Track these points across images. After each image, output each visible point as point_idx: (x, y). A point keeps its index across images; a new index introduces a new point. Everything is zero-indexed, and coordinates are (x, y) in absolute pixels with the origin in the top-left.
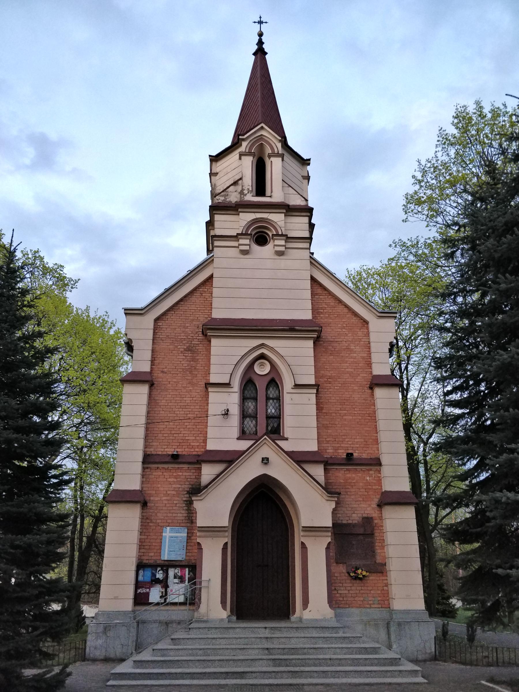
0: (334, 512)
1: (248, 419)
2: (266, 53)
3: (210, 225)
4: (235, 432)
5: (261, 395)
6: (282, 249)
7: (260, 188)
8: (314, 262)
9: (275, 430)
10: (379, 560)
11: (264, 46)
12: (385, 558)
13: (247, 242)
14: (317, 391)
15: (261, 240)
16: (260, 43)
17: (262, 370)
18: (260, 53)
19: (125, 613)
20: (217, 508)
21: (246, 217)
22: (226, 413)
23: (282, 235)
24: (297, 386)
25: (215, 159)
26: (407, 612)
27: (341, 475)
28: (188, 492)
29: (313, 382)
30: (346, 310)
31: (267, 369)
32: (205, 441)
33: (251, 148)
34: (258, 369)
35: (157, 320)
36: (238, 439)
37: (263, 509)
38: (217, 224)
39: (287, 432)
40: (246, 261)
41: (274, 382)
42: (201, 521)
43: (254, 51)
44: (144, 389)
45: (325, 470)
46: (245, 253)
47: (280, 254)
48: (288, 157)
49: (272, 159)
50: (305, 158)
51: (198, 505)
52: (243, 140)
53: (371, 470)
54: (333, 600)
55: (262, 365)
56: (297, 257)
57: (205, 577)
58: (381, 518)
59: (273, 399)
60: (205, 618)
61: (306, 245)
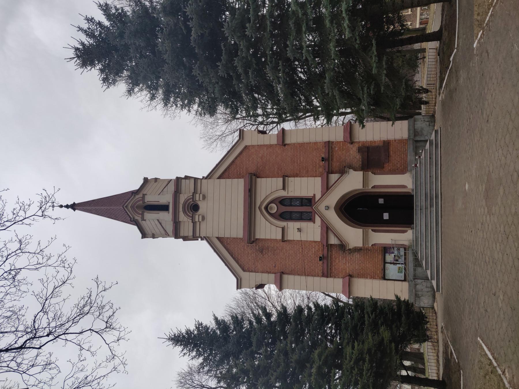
0: (355, 170)
1: (303, 217)
2: (74, 203)
3: (185, 239)
4: (310, 224)
5: (296, 209)
6: (201, 195)
7: (164, 208)
8: (209, 176)
9: (309, 201)
10: (381, 144)
11: (69, 204)
12: (380, 141)
13: (197, 217)
14: (286, 176)
15: (195, 208)
16: (67, 206)
17: (274, 208)
18: (74, 207)
19: (409, 286)
20: (353, 235)
21: (182, 217)
22: (299, 230)
23: (193, 195)
24: (284, 188)
25: (144, 235)
26: (409, 130)
27: (336, 165)
28: (344, 252)
29: (282, 179)
30: (239, 158)
31: (273, 205)
32: (315, 242)
33: (139, 214)
34: (274, 211)
35: (244, 270)
36: (314, 223)
37: (360, 209)
38: (186, 235)
39: (310, 194)
40: (209, 218)
41: (282, 201)
42: (360, 244)
43: (72, 210)
44: (285, 277)
45: (332, 173)
46: (203, 218)
47: (204, 197)
48: (144, 191)
49: (146, 201)
50: (141, 182)
51: (351, 247)
52: (134, 218)
53: (332, 147)
54: (402, 172)
55: (271, 208)
56: (208, 187)
57: (390, 242)
58: (359, 142)
59: (291, 202)
60: (411, 241)
61: (199, 181)
